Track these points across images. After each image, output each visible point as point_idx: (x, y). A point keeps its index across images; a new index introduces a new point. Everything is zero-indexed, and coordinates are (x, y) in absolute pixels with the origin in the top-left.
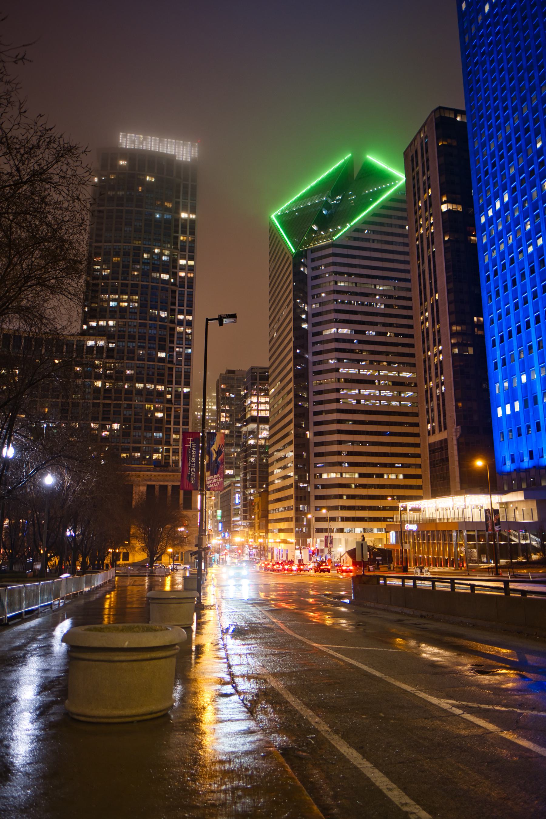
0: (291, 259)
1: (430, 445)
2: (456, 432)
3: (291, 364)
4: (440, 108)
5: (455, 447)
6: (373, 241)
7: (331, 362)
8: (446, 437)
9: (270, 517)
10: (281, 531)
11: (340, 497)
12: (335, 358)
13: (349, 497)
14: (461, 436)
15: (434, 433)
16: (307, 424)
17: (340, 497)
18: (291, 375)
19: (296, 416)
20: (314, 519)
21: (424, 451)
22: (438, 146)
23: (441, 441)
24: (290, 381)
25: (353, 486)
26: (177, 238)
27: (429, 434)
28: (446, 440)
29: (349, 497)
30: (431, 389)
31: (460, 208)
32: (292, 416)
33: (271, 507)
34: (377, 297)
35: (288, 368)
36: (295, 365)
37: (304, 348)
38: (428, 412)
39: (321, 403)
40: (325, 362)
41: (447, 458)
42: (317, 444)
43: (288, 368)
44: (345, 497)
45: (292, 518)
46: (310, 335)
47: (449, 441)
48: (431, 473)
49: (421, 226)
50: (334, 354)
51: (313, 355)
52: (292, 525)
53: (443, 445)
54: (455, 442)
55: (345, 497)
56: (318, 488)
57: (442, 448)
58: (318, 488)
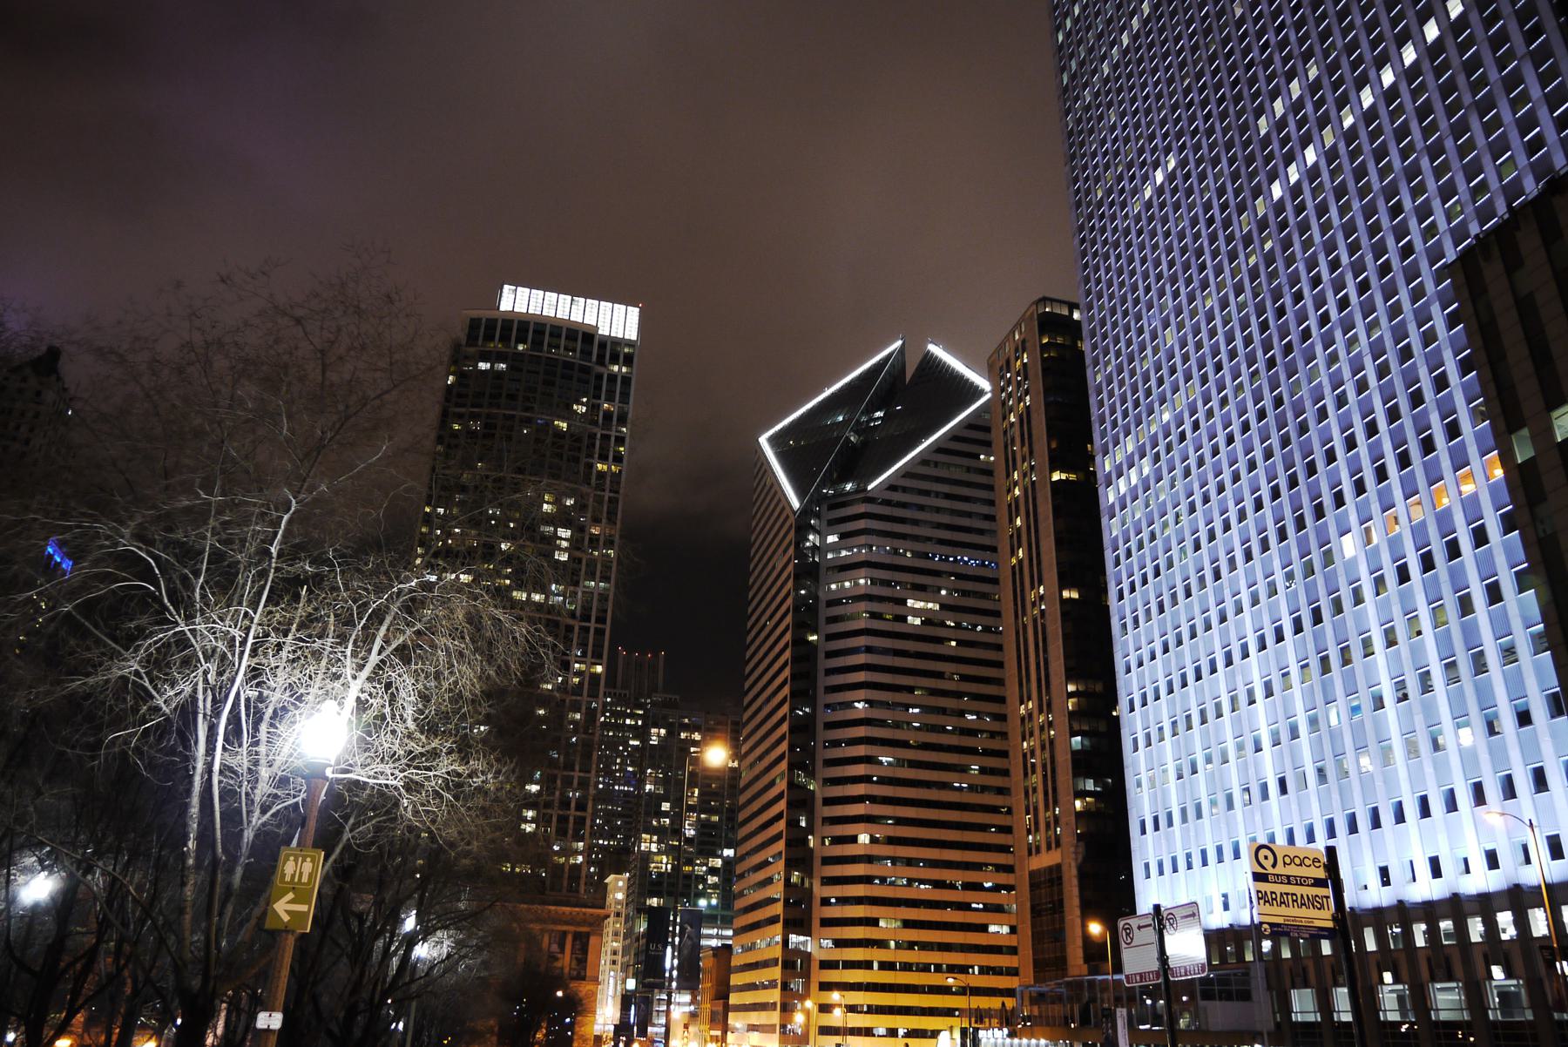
0: (792, 520)
1: (1032, 874)
2: (1076, 853)
3: (785, 709)
4: (1044, 300)
5: (1075, 882)
6: (936, 464)
7: (860, 705)
8: (1059, 860)
9: (734, 999)
10: (752, 1028)
11: (867, 965)
12: (866, 701)
13: (885, 966)
14: (1085, 860)
15: (1038, 851)
16: (807, 985)
17: (867, 965)
18: (785, 727)
19: (789, 804)
20: (816, 1009)
21: (1021, 879)
22: (1044, 360)
23: (1050, 869)
24: (782, 738)
25: (892, 944)
26: (591, 466)
27: (1030, 854)
28: (1059, 866)
29: (885, 966)
30: (1041, 711)
31: (1073, 477)
32: (782, 805)
33: (736, 979)
34: (943, 592)
35: (780, 714)
36: (792, 709)
37: (808, 871)
38: (1027, 793)
39: (836, 744)
40: (849, 705)
41: (1061, 901)
42: (829, 802)
43: (780, 714)
44: (876, 965)
45: (775, 1004)
46: (821, 655)
47: (1064, 868)
48: (1033, 926)
49: (1016, 484)
50: (862, 693)
51: (823, 884)
52: (774, 1017)
53: (1053, 876)
54: (1074, 872)
55: (876, 965)
56: (830, 904)
57: (1051, 881)
58: (830, 904)
